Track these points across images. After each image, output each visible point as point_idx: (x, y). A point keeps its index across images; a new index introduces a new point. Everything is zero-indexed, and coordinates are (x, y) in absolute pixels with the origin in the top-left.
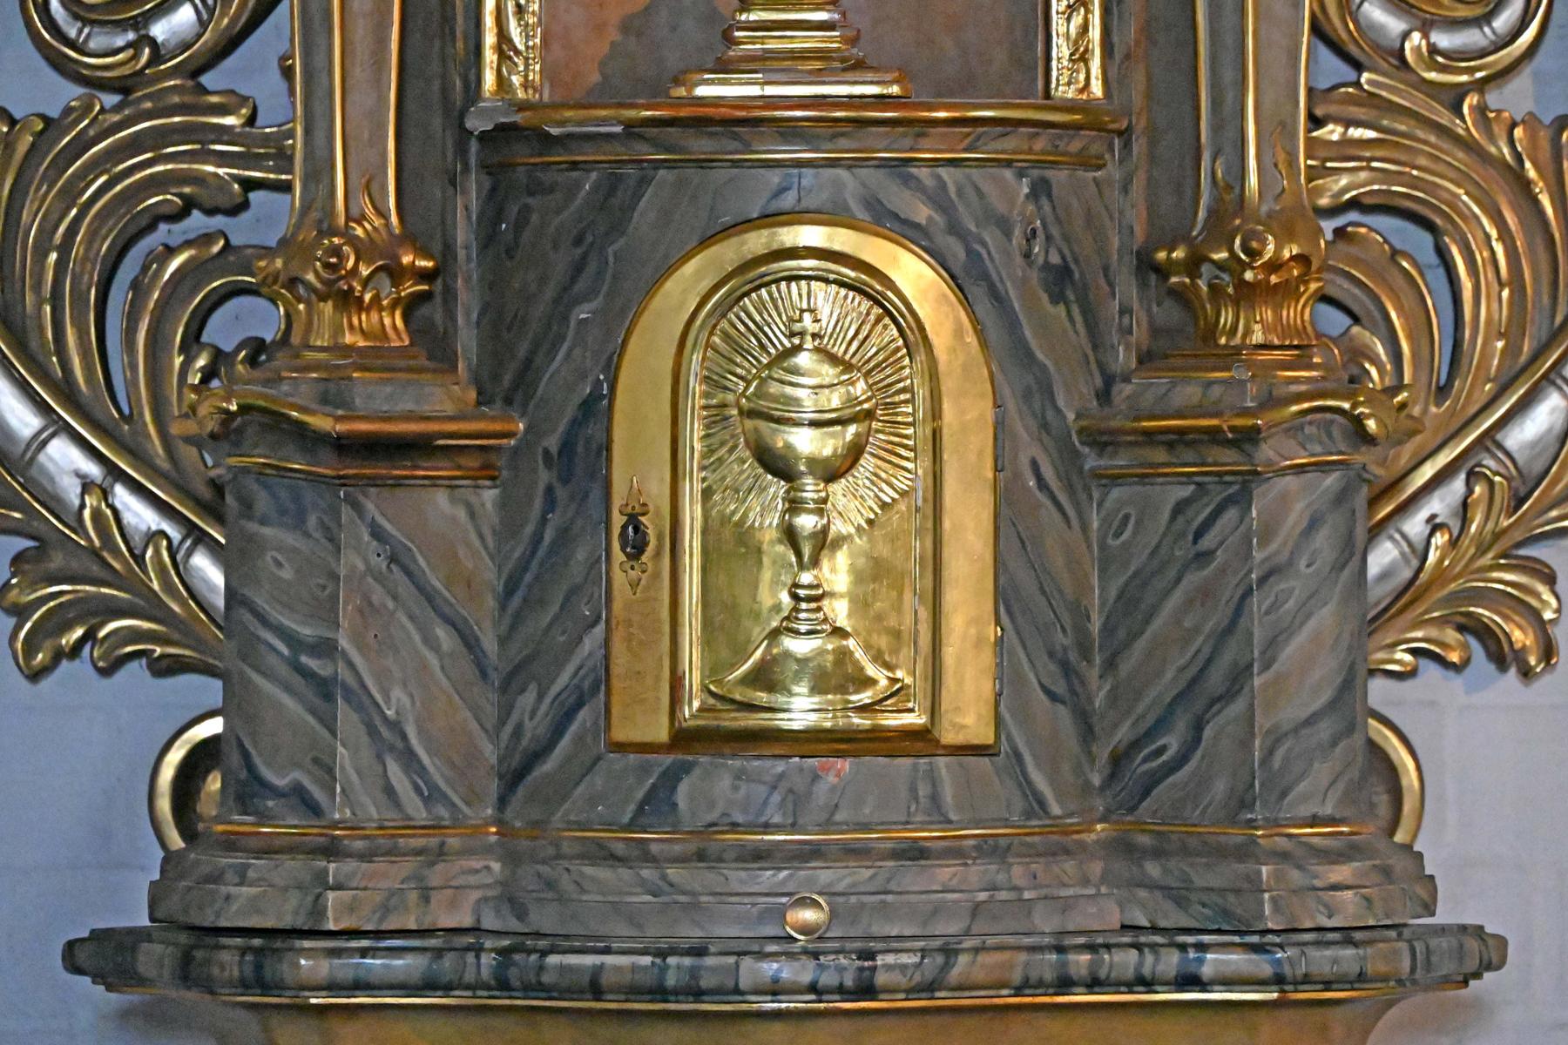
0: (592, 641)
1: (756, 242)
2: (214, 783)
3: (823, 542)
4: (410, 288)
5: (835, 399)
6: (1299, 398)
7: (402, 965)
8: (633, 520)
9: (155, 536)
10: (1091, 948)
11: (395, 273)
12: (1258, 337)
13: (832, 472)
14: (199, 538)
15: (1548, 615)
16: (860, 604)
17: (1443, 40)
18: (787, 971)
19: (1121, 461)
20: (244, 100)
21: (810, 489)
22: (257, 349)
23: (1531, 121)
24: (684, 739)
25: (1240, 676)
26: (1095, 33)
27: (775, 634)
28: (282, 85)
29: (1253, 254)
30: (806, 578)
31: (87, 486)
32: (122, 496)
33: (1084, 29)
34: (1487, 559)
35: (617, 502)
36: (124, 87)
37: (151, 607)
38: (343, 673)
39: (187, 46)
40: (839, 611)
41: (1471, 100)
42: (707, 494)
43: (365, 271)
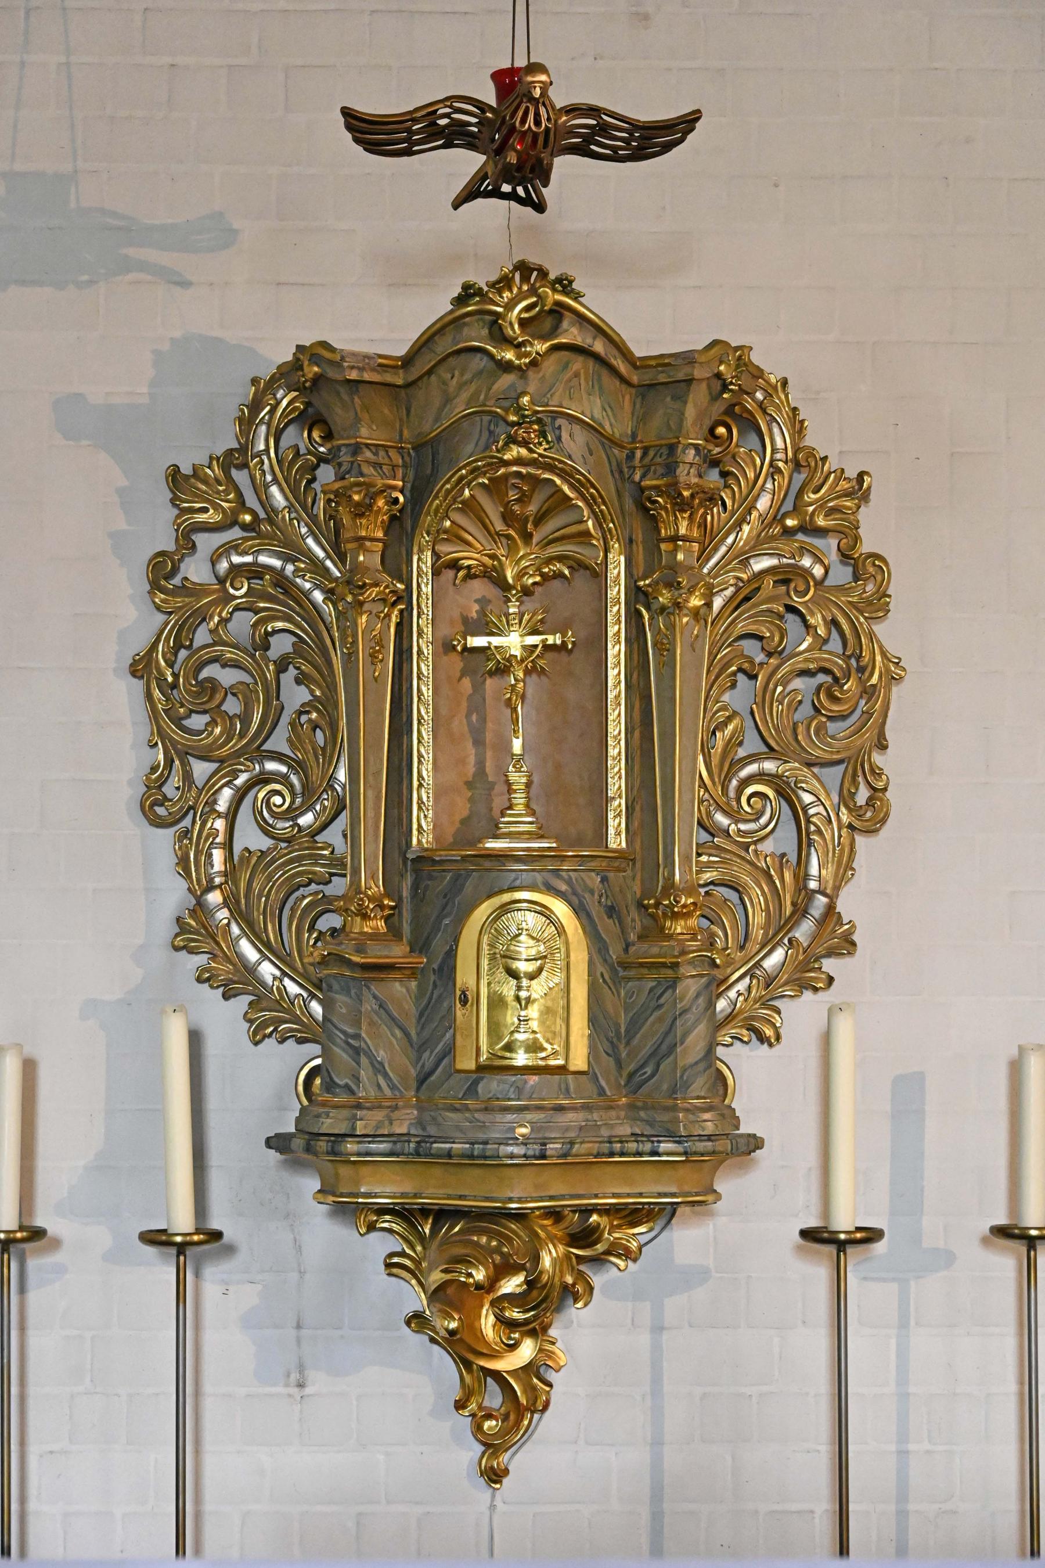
0: (448, 1035)
1: (506, 897)
2: (318, 1081)
3: (529, 1000)
4: (387, 912)
5: (533, 952)
8: (463, 993)
9: (298, 996)
10: (621, 1142)
12: (679, 930)
13: (532, 977)
14: (313, 996)
15: (778, 1025)
16: (542, 1022)
17: (743, 827)
19: (632, 973)
21: (525, 982)
22: (334, 931)
23: (773, 854)
24: (481, 1069)
25: (672, 1048)
26: (623, 825)
27: (512, 1032)
30: (523, 1013)
31: (275, 978)
32: (287, 982)
37: (296, 1020)
40: (534, 1025)
41: (752, 847)
42: (489, 984)
43: (371, 906)
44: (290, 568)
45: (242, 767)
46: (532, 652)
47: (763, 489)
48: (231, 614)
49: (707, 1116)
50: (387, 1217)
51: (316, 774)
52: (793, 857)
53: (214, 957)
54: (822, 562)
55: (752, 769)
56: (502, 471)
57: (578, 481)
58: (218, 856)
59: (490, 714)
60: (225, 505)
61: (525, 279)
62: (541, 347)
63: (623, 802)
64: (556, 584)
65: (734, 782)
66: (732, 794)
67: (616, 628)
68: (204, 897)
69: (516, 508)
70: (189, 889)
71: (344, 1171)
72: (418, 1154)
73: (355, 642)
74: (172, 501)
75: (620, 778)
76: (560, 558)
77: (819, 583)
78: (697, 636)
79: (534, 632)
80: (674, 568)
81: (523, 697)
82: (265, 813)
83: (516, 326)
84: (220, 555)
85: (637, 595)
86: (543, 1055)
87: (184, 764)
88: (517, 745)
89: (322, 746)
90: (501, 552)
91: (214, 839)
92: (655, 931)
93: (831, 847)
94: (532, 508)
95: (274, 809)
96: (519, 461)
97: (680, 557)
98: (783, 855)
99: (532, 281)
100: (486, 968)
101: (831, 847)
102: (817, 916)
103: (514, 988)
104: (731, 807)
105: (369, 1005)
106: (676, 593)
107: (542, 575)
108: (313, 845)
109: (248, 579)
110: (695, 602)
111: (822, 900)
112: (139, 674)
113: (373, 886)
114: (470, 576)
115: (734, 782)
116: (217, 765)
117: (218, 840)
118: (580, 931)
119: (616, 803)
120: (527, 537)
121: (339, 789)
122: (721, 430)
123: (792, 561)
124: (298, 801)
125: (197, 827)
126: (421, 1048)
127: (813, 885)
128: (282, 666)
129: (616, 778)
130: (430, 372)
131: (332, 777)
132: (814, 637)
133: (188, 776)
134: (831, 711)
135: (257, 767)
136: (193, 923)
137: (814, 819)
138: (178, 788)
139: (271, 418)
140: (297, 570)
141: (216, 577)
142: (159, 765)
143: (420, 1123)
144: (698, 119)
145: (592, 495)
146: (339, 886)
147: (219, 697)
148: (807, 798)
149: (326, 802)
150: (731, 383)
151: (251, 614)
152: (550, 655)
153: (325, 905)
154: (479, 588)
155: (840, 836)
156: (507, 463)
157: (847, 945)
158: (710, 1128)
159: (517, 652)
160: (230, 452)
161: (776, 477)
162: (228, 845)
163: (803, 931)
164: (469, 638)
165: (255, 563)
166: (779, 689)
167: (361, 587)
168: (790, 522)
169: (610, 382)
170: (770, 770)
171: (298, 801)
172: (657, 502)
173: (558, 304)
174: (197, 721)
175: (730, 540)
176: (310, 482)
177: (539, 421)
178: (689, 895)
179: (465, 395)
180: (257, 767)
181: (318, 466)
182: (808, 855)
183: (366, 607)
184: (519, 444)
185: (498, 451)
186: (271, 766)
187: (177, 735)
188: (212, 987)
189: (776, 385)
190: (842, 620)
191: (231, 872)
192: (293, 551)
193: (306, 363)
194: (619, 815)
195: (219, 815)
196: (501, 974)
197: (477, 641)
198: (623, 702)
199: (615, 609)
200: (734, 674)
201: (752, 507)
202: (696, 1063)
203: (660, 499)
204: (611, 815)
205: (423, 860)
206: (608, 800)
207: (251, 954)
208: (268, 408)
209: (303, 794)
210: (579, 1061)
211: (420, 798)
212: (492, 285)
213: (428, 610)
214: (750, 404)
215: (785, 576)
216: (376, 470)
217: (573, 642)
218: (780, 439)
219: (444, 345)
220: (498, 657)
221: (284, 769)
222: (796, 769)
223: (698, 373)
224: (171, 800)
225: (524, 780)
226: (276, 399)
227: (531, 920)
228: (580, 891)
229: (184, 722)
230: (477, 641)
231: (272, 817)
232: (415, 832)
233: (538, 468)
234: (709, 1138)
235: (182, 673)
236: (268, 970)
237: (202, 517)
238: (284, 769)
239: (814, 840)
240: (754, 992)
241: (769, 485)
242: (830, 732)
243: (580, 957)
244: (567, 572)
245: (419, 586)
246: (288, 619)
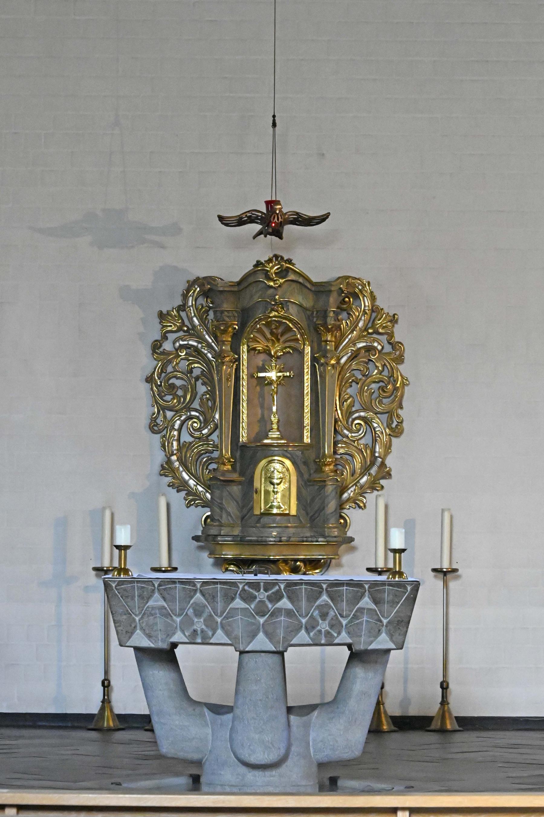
0: (251, 503)
1: (270, 459)
2: (209, 520)
3: (277, 492)
4: (231, 463)
5: (279, 476)
6: (331, 477)
7: (229, 539)
8: (256, 489)
9: (202, 491)
10: (306, 538)
11: (230, 461)
12: (327, 470)
13: (278, 484)
14: (207, 492)
15: (365, 502)
16: (282, 499)
17: (353, 435)
18: (272, 539)
19: (311, 484)
20: (213, 440)
21: (276, 486)
22: (214, 469)
23: (363, 444)
24: (262, 514)
25: (324, 508)
26: (309, 435)
27: (272, 503)
28: (217, 438)
29: (326, 461)
30: (275, 496)
31: (194, 485)
32: (198, 486)
33: (308, 434)
34: (357, 496)
35: (254, 488)
36: (199, 438)
37: (201, 499)
38: (224, 506)
39: (206, 434)
40: (279, 500)
41: (356, 442)
42: (264, 487)
43: (227, 461)
44: (200, 346)
45: (183, 414)
46: (280, 378)
47: (361, 319)
48: (180, 361)
49: (336, 530)
50: (232, 566)
51: (208, 416)
52: (370, 444)
53: (174, 478)
54: (381, 345)
55: (357, 415)
56: (270, 319)
57: (295, 323)
58: (175, 444)
59: (266, 398)
60: (178, 324)
61: (277, 259)
62: (281, 281)
63: (309, 427)
64: (288, 355)
65: (350, 420)
66: (350, 423)
67: (307, 370)
68: (171, 458)
69: (274, 330)
70: (165, 455)
71: (218, 547)
72: (241, 541)
73: (221, 375)
74: (160, 323)
75: (308, 419)
76: (289, 347)
77: (380, 352)
78: (333, 373)
79: (280, 372)
80: (326, 351)
81: (277, 393)
82: (191, 429)
83: (274, 275)
84: (176, 341)
85: (314, 359)
86: (282, 509)
87: (164, 412)
88: (274, 409)
89: (210, 406)
90: (270, 345)
91: (174, 438)
92: (319, 470)
93: (383, 441)
94: (280, 331)
95: (194, 428)
96: (275, 316)
97: (328, 347)
98: (367, 444)
99: (279, 260)
100: (263, 481)
101: (383, 441)
102: (378, 465)
103: (272, 488)
104: (349, 428)
105: (225, 494)
106: (327, 359)
107: (284, 352)
108: (207, 440)
109: (185, 349)
110: (333, 362)
111: (380, 460)
112: (148, 382)
113: (227, 455)
114: (259, 352)
115: (350, 420)
116: (175, 412)
117: (175, 438)
118: (294, 470)
119: (307, 428)
120: (278, 340)
121: (216, 421)
122: (347, 299)
123: (371, 344)
124: (202, 425)
125: (168, 434)
126: (243, 507)
127: (377, 455)
128: (197, 379)
129: (307, 419)
130: (246, 287)
131: (214, 417)
132: (378, 370)
133: (165, 417)
134: (383, 395)
135: (188, 413)
136: (167, 467)
137: (378, 432)
138: (162, 421)
139: (193, 295)
140: (202, 346)
141: (175, 349)
142: (155, 413)
143: (242, 531)
144: (329, 215)
145: (299, 327)
146: (216, 454)
147: (176, 390)
148: (375, 425)
149: (212, 426)
150: (345, 291)
151: (186, 361)
152: (286, 379)
153: (211, 460)
154: (263, 356)
155: (386, 438)
156: (271, 317)
157: (388, 475)
158: (336, 533)
159: (274, 378)
160: (179, 306)
161: (365, 315)
162: (179, 440)
163: (374, 471)
164: (259, 373)
165: (188, 344)
166: (366, 388)
167: (223, 357)
168: (370, 331)
169: (305, 290)
170: (363, 415)
171: (202, 425)
172: (321, 329)
173: (287, 267)
174: (168, 398)
175: (350, 337)
176: (207, 316)
177: (282, 304)
178: (330, 458)
179: (258, 295)
180: (188, 413)
181: (209, 310)
182: (375, 444)
183: (225, 364)
184: (275, 311)
185: (268, 313)
186: (193, 413)
187: (161, 402)
188: (173, 488)
189: (366, 284)
190: (387, 364)
191: (179, 449)
192: (201, 339)
193: (206, 284)
194: (308, 432)
195: (176, 430)
196: (268, 483)
197: (261, 375)
198: (309, 394)
199: (307, 363)
200: (351, 382)
201: (357, 325)
202: (332, 513)
203: (321, 328)
204: (305, 431)
205: (244, 447)
206: (304, 427)
207: (186, 477)
208: (193, 291)
209: (204, 422)
210: (293, 512)
211: (243, 426)
212: (265, 261)
213: (245, 363)
214: (357, 290)
215: (369, 349)
216: (228, 318)
217: (293, 375)
218: (366, 303)
219: (251, 279)
220: (268, 380)
221: (197, 414)
222: (371, 415)
223: (333, 289)
224: (159, 425)
225: (277, 420)
226: (195, 288)
227: (278, 466)
228: (294, 457)
229: (164, 398)
230: (261, 375)
231: (194, 430)
232: (241, 437)
233: (282, 319)
234: (335, 537)
235: (163, 381)
236: (192, 483)
237: (169, 328)
238: (197, 414)
239: (377, 439)
240: (356, 491)
241: (363, 318)
242: (384, 403)
243: (294, 479)
244: (291, 351)
245: (243, 356)
246: (198, 363)
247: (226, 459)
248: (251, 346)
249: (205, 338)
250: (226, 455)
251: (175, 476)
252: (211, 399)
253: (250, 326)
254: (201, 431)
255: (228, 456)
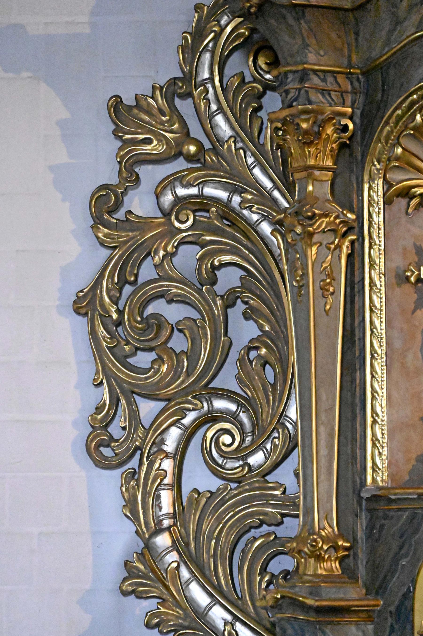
4: (341, 553)
11: (336, 548)
22: (286, 573)
28: (295, 480)
43: (325, 547)
44: (236, 199)
45: (190, 406)
48: (177, 247)
60: (169, 135)
70: (137, 532)
74: (114, 133)
82: (215, 453)
84: (164, 188)
87: (131, 403)
95: (223, 448)
109: (194, 211)
113: (327, 526)
117: (166, 481)
124: (248, 440)
135: (205, 405)
136: (142, 567)
138: (124, 428)
140: (244, 201)
147: (166, 333)
149: (277, 441)
165: (201, 196)
167: (310, 218)
171: (248, 440)
179: (415, 18)
180: (205, 405)
183: (316, 238)
195: (167, 456)
208: (212, 35)
211: (374, 434)
216: (323, 94)
221: (233, 407)
224: (117, 441)
226: (220, 26)
231: (222, 456)
232: (369, 471)
238: (233, 407)
245: (370, 215)
246: (234, 251)
247: (325, 540)
248: (398, 184)
249: (252, 174)
250: (324, 529)
251: (167, 596)
252: (272, 359)
253: (393, 119)
254: (244, 458)
255: (330, 530)
